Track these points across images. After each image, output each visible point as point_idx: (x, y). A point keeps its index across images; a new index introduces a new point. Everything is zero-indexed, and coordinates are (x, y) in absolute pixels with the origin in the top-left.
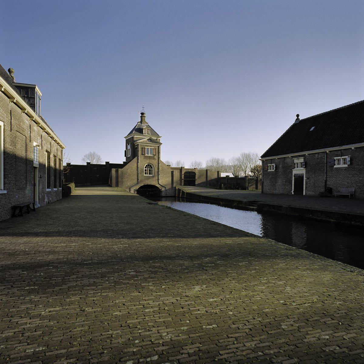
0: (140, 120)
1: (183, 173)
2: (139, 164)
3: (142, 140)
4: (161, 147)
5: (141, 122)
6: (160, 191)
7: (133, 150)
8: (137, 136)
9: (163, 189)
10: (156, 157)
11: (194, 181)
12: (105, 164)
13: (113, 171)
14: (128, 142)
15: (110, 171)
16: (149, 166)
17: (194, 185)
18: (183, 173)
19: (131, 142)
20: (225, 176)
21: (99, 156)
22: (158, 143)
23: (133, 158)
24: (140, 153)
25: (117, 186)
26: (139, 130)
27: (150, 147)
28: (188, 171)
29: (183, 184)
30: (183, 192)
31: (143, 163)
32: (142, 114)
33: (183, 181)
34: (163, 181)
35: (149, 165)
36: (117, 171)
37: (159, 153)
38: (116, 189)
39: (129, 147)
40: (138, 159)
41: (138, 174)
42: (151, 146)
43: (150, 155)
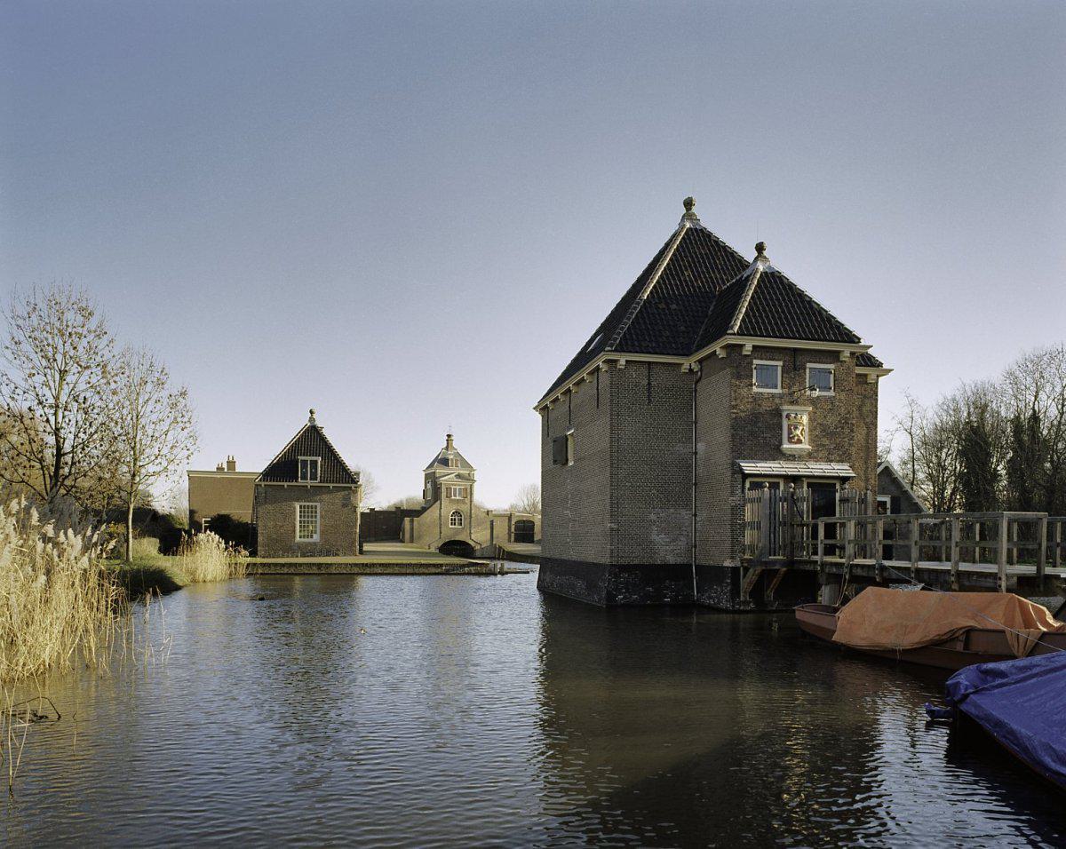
0: (445, 446)
1: (513, 523)
2: (442, 510)
3: (447, 477)
4: (475, 485)
5: (447, 448)
6: (472, 548)
7: (434, 489)
8: (440, 471)
9: (478, 547)
10: (467, 501)
11: (532, 536)
12: (539, 566)
13: (407, 520)
14: (427, 476)
15: (402, 520)
16: (457, 513)
17: (532, 542)
18: (513, 523)
19: (431, 478)
20: (368, 511)
21: (370, 474)
22: (469, 479)
23: (435, 502)
24: (444, 495)
25: (412, 541)
26: (444, 462)
27: (461, 485)
28: (521, 519)
29: (513, 539)
30: (504, 551)
31: (447, 508)
32: (449, 436)
33: (513, 535)
34: (478, 537)
35: (456, 512)
36: (412, 521)
37: (471, 494)
38: (410, 544)
39: (429, 486)
40: (441, 504)
41: (441, 525)
42: (459, 485)
43: (458, 498)
